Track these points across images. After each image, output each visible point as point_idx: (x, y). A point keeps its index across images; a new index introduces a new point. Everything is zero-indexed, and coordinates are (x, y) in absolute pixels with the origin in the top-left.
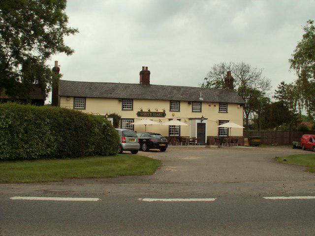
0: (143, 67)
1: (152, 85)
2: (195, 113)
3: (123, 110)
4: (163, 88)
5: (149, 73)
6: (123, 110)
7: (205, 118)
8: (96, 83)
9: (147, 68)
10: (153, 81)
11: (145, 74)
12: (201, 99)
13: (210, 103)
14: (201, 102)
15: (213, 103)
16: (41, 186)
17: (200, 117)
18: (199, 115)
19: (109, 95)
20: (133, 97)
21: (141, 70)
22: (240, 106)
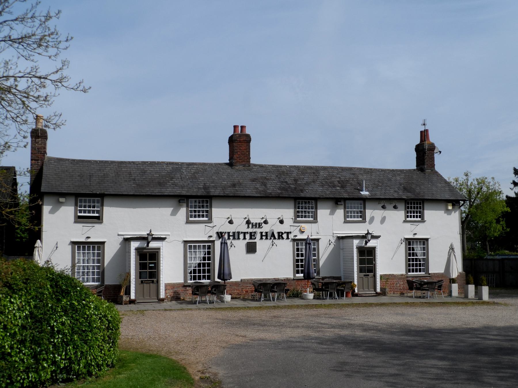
0: (235, 127)
1: (255, 165)
2: (409, 224)
3: (346, 222)
4: (280, 171)
5: (247, 139)
6: (346, 222)
7: (375, 234)
8: (130, 163)
9: (243, 127)
10: (259, 155)
11: (239, 142)
12: (365, 193)
13: (384, 202)
14: (364, 200)
15: (390, 200)
16: (340, 333)
17: (363, 232)
18: (360, 229)
19: (157, 191)
20: (213, 192)
21: (231, 133)
22: (453, 205)
